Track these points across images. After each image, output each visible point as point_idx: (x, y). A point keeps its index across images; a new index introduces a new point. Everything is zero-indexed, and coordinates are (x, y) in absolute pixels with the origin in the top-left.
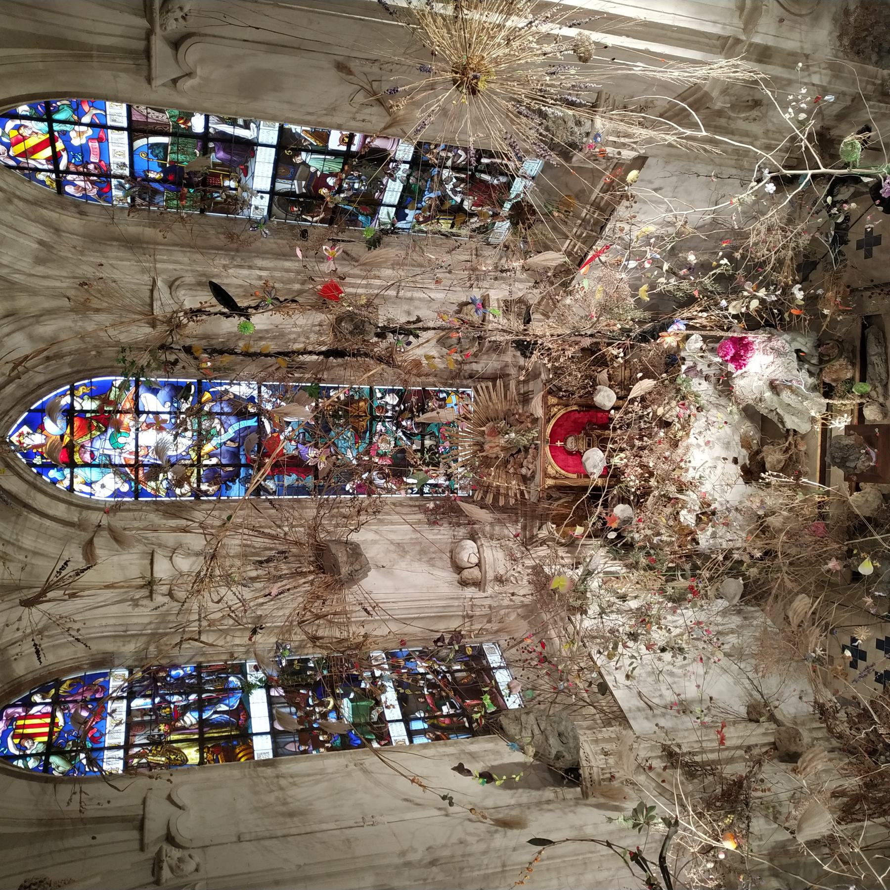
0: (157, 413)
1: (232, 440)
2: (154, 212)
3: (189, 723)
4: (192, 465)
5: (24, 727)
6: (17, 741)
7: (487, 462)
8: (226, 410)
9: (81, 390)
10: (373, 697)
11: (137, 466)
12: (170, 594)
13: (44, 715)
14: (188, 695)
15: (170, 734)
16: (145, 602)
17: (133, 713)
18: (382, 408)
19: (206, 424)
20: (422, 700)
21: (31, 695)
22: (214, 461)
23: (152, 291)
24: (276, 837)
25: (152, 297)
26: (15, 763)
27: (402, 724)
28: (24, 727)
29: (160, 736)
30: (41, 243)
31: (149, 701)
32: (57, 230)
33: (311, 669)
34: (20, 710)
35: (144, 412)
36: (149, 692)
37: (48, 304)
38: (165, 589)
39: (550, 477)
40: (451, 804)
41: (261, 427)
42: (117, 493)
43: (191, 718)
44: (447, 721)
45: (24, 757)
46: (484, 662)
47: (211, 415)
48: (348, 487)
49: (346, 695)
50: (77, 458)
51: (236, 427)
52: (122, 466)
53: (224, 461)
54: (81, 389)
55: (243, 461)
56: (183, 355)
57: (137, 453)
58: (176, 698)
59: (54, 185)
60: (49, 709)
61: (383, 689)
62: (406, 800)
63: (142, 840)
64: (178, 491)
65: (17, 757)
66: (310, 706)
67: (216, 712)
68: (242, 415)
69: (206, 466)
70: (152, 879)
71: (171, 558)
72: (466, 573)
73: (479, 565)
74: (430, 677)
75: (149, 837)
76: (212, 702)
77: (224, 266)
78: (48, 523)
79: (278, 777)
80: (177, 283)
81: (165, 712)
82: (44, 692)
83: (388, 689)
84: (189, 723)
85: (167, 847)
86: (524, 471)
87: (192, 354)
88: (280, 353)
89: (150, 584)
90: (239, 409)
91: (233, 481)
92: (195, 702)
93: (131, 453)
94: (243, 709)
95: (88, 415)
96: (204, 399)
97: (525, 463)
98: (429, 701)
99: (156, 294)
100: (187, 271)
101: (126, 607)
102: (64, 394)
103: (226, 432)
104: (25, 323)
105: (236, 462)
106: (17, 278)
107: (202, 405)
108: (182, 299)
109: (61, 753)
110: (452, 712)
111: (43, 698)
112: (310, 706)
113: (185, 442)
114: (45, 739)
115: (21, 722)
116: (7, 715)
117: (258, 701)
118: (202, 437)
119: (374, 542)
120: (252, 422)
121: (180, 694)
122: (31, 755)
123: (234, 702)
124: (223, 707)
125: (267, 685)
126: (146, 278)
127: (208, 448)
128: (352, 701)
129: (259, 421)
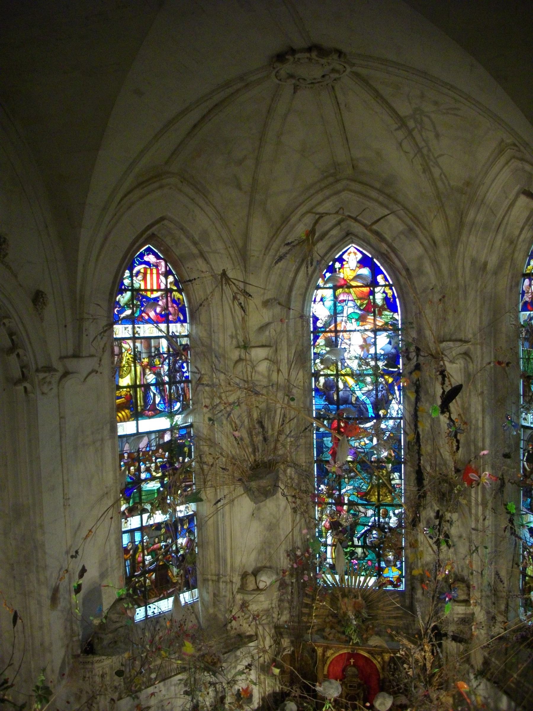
0: (375, 344)
1: (357, 398)
4: (337, 371)
5: (152, 273)
6: (142, 271)
7: (334, 601)
8: (380, 394)
9: (389, 292)
10: (160, 502)
11: (336, 331)
12: (240, 360)
13: (159, 285)
14: (169, 376)
15: (141, 366)
16: (234, 342)
17: (157, 340)
18: (386, 515)
19: (368, 379)
20: (157, 540)
21: (173, 275)
22: (341, 385)
23: (461, 340)
24: (61, 440)
25: (456, 340)
26: (127, 271)
27: (139, 526)
28: (152, 273)
29: (140, 360)
30: (485, 264)
31: (165, 350)
32: (495, 273)
33: (184, 460)
35: (375, 335)
36: (171, 350)
37: (444, 268)
38: (243, 356)
39: (324, 652)
40: (72, 557)
41: (369, 420)
42: (316, 319)
43: (151, 378)
44: (140, 559)
45: (131, 276)
47: (376, 384)
48: (322, 487)
49: (163, 485)
50: (340, 291)
51: (368, 401)
52: (336, 322)
53: (341, 393)
54: (390, 291)
55: (341, 407)
56: (414, 362)
57: (346, 331)
58: (166, 368)
59: (528, 272)
60: (163, 287)
61: (164, 512)
62: (79, 525)
63: (67, 357)
64: (318, 361)
65: (131, 273)
66: (156, 459)
67: (154, 395)
68: (377, 406)
69: (338, 381)
70: (40, 367)
71: (266, 359)
72: (251, 579)
73: (258, 589)
75: (68, 362)
76: (161, 392)
77: (482, 393)
78: (291, 275)
79: (102, 440)
80: (467, 358)
81: (157, 361)
83: (165, 516)
85: (58, 375)
86: (328, 630)
87: (414, 370)
88: (418, 435)
89: (246, 346)
90: (381, 403)
91: (326, 400)
92: (162, 380)
93: (345, 327)
94: (156, 413)
95: (371, 297)
96: (387, 377)
97: (333, 631)
98: (155, 546)
99: (458, 344)
100: (477, 365)
101: (231, 330)
102: (386, 280)
103: (362, 392)
104: (431, 253)
105: (341, 402)
106: (461, 248)
107: (382, 376)
108: (457, 362)
109: (132, 298)
110: (147, 563)
111: (171, 283)
112: (156, 460)
113: (354, 365)
115: (155, 271)
116: (160, 262)
117: (161, 423)
118: (359, 377)
119: (278, 506)
120: (371, 413)
121: (169, 370)
122: (132, 280)
123: (161, 407)
124: (158, 399)
125: (172, 429)
126: (470, 336)
127: (351, 381)
128: (158, 490)
129: (372, 418)
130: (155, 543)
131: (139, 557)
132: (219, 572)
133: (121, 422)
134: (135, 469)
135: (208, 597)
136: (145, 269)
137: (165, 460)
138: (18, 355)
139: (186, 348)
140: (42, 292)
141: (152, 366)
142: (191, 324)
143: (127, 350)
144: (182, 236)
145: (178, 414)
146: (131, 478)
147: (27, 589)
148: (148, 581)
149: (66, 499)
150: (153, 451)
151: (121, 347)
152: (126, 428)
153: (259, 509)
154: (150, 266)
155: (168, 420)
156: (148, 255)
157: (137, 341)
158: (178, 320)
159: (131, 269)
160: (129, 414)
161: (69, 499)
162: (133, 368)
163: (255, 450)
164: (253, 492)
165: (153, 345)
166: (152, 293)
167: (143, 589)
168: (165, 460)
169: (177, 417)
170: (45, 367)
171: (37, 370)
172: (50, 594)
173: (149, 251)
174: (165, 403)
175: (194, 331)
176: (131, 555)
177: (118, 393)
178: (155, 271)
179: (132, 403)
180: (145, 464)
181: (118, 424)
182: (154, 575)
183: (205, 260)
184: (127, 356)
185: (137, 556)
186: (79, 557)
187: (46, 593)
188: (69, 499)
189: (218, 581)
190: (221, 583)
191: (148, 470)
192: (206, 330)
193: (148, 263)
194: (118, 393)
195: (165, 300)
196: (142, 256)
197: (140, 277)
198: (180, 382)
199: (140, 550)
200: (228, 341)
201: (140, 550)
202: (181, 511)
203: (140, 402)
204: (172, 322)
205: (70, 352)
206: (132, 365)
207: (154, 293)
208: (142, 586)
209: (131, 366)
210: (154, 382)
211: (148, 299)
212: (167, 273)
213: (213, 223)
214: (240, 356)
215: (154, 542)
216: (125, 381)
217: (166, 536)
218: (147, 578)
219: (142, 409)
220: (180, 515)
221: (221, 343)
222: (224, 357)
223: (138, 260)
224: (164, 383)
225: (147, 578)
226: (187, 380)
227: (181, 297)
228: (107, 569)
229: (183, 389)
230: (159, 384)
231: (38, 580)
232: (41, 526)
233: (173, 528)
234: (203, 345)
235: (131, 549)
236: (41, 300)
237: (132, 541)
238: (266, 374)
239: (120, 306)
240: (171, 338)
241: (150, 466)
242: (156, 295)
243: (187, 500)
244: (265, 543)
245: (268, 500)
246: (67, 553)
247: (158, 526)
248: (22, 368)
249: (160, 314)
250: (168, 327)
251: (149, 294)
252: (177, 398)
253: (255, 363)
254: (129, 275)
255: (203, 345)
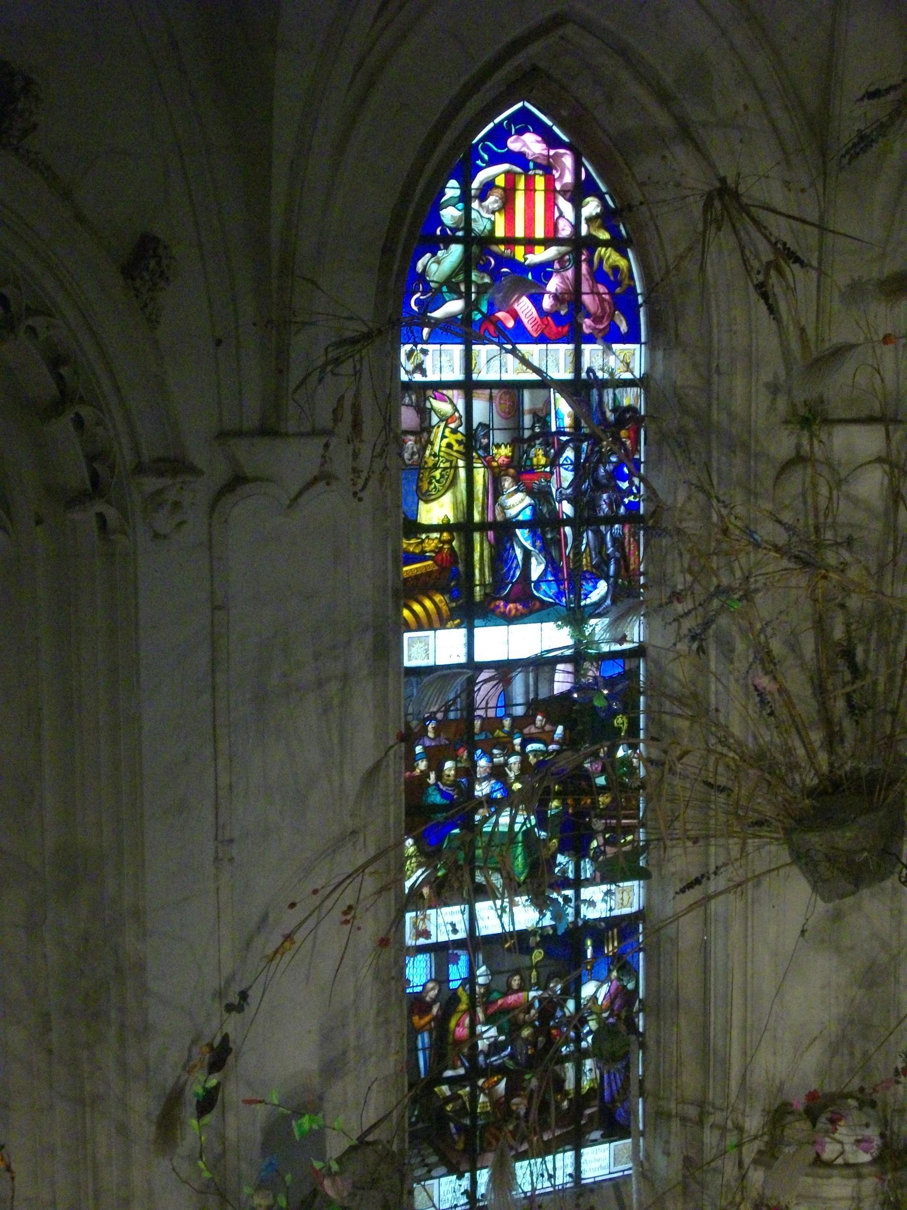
2: (646, 567)
3: (510, 502)
6: (500, 181)
12: (799, 459)
13: (552, 225)
15: (488, 466)
16: (782, 404)
17: (542, 393)
20: (516, 982)
21: (601, 197)
28: (530, 189)
29: (486, 448)
31: (567, 422)
34: (568, 178)
43: (518, 504)
44: (462, 1032)
45: (465, 198)
46: (596, 1135)
58: (567, 476)
60: (565, 231)
61: (540, 902)
62: (264, 919)
63: (240, 434)
67: (527, 555)
72: (798, 1128)
74: (571, 1005)
75: (241, 448)
81: (539, 457)
82: (606, 218)
84: (510, 502)
89: (811, 418)
94: (530, 608)
98: (512, 999)
109: (466, 265)
110: (482, 1045)
111: (589, 220)
112: (524, 745)
114: (500, 232)
115: (540, 182)
117: (553, 637)
122: (468, 210)
123: (546, 592)
124: (537, 569)
125: (578, 658)
130: (509, 991)
131: (459, 1026)
132: (705, 1092)
133: (420, 627)
134: (457, 769)
135: (667, 1167)
136: (510, 177)
137: (552, 747)
138: (79, 422)
139: (626, 415)
140: (155, 239)
141: (520, 470)
142: (652, 346)
143: (445, 419)
144: (624, 75)
145: (599, 616)
146: (444, 795)
147: (88, 1087)
148: (482, 1098)
149: (223, 840)
150: (515, 719)
151: (424, 412)
152: (436, 647)
153: (837, 916)
154: (526, 169)
155: (567, 630)
156: (520, 132)
157: (477, 393)
158: (612, 337)
159: (465, 176)
160: (444, 608)
161: (231, 841)
162: (462, 473)
163: (833, 739)
164: (816, 865)
165: (527, 405)
166: (529, 251)
167: (467, 1122)
168: (552, 747)
169: (593, 621)
170: (160, 460)
171: (140, 469)
172: (156, 1110)
173: (524, 122)
174: (559, 582)
175: (660, 368)
176: (434, 1019)
177: (410, 545)
178: (540, 182)
179: (456, 575)
180: (491, 757)
181: (406, 636)
182: (502, 1085)
183: (699, 149)
184: (443, 440)
185: (453, 1023)
186: (250, 1011)
187: (143, 1105)
188: (231, 841)
189: (701, 1123)
190: (707, 1131)
191: (498, 773)
192: (695, 366)
193: (519, 159)
194: (410, 545)
195: (569, 273)
196: (500, 135)
197: (493, 201)
198: (610, 521)
199: (463, 1006)
200: (762, 401)
201: (463, 1006)
202: (592, 903)
203: (481, 573)
204: (591, 339)
205: (252, 420)
206: (461, 463)
207: (538, 249)
208: (461, 1111)
209: (456, 468)
210: (526, 515)
211: (519, 268)
212: (580, 192)
213: (724, 33)
214: (798, 446)
215: (509, 985)
216: (437, 511)
217: (545, 972)
218: (482, 1089)
219: (486, 595)
220: (589, 913)
221: (738, 405)
222: (745, 447)
223: (487, 149)
224: (558, 522)
225: (482, 1089)
226: (632, 516)
227: (622, 263)
228: (344, 1053)
229: (618, 542)
230: (543, 523)
231: (123, 1065)
232: (137, 914)
233: (567, 949)
234: (685, 411)
235: (434, 1001)
236: (152, 264)
237: (441, 977)
238: (878, 504)
239: (427, 289)
240: (580, 388)
241: (506, 764)
242: (541, 255)
243: (610, 874)
244: (851, 1022)
245: (865, 892)
246: (220, 994)
247: (521, 940)
248: (91, 458)
249: (554, 315)
250: (578, 355)
251: (519, 252)
252: (597, 566)
253: (843, 473)
254: (457, 192)
255: (685, 411)
